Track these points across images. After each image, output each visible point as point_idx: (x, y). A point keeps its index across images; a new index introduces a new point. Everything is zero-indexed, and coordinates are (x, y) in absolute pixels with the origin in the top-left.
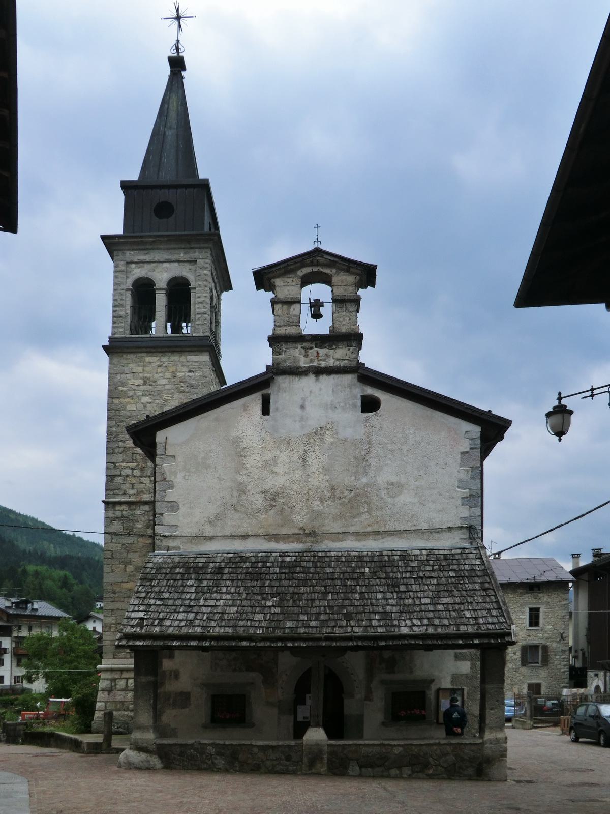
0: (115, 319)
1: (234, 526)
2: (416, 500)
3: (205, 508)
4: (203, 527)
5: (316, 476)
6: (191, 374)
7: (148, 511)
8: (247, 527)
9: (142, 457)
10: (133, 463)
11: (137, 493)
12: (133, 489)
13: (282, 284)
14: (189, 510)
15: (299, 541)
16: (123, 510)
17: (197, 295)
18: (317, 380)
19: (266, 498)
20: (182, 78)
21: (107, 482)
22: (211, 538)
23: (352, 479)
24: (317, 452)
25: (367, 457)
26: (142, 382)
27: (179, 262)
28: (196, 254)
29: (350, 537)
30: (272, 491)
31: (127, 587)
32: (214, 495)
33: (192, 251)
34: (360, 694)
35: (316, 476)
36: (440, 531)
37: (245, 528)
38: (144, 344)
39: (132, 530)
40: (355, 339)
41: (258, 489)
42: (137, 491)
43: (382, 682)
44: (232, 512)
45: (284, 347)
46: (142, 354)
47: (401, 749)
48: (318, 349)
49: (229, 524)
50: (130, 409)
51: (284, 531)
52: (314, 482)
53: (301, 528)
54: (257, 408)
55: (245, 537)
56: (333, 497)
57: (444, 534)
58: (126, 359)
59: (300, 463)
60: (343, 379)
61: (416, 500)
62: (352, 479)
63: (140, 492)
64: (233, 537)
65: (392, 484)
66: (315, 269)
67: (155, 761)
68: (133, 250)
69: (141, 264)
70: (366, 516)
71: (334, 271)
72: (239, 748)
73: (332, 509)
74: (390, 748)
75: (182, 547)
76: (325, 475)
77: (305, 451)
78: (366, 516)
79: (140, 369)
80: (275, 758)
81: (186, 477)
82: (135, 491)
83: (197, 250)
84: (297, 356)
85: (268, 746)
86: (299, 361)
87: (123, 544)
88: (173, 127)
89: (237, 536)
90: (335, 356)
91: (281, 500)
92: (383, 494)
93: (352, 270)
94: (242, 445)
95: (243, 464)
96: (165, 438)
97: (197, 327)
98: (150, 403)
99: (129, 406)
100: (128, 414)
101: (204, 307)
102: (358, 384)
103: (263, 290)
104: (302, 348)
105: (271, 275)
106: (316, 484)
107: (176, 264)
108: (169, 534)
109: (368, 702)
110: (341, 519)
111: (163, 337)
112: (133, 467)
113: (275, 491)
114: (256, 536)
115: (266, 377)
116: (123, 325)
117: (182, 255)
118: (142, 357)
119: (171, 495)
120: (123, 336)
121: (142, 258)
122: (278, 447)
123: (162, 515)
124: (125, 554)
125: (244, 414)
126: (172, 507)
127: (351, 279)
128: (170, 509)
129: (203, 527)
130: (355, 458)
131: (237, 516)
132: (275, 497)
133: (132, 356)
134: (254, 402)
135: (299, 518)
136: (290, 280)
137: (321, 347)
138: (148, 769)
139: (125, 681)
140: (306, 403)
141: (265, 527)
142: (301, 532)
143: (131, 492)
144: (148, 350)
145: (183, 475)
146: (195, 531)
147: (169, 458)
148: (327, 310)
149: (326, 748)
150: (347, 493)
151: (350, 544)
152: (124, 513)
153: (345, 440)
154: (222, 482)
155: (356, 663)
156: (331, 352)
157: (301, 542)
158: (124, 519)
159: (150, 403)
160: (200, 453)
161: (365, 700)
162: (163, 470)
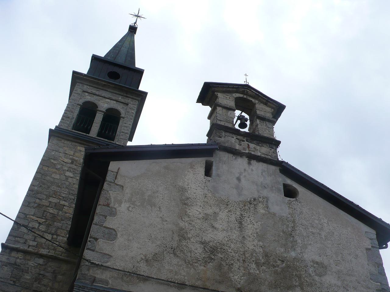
0: (64, 118)
1: (171, 271)
2: (339, 283)
3: (143, 244)
4: (138, 265)
5: (251, 239)
7: (41, 265)
8: (184, 276)
9: (51, 216)
10: (43, 219)
11: (36, 246)
12: (34, 241)
13: (223, 97)
14: (126, 242)
16: (18, 258)
17: (124, 122)
18: (249, 163)
19: (205, 249)
25: (293, 234)
27: (117, 101)
30: (211, 244)
32: (155, 233)
33: (127, 98)
35: (251, 239)
41: (198, 239)
42: (37, 244)
44: (171, 255)
46: (76, 144)
48: (250, 144)
49: (167, 267)
50: (55, 177)
52: (250, 245)
54: (202, 171)
58: (64, 143)
59: (237, 225)
60: (269, 167)
63: (39, 245)
65: (317, 263)
66: (245, 97)
69: (92, 95)
71: (257, 102)
75: (110, 282)
76: (259, 241)
77: (241, 215)
81: (130, 209)
83: (130, 99)
89: (174, 283)
92: (311, 270)
93: (269, 104)
96: (118, 168)
97: (120, 140)
98: (71, 178)
99: (54, 175)
100: (52, 180)
103: (201, 104)
104: (236, 138)
105: (216, 89)
106: (252, 247)
107: (115, 102)
108: (100, 263)
111: (95, 138)
112: (41, 222)
113: (214, 244)
116: (69, 123)
117: (120, 98)
118: (76, 146)
119: (111, 223)
120: (67, 129)
122: (218, 205)
123: (96, 239)
125: (190, 170)
128: (106, 236)
129: (138, 265)
131: (175, 261)
132: (214, 250)
134: (199, 163)
135: (236, 277)
141: (203, 280)
144: (82, 142)
145: (128, 206)
146: (129, 267)
147: (117, 187)
150: (279, 262)
152: (18, 260)
153: (274, 214)
154: (164, 223)
156: (258, 148)
158: (16, 267)
159: (71, 178)
160: (147, 190)
162: (109, 196)
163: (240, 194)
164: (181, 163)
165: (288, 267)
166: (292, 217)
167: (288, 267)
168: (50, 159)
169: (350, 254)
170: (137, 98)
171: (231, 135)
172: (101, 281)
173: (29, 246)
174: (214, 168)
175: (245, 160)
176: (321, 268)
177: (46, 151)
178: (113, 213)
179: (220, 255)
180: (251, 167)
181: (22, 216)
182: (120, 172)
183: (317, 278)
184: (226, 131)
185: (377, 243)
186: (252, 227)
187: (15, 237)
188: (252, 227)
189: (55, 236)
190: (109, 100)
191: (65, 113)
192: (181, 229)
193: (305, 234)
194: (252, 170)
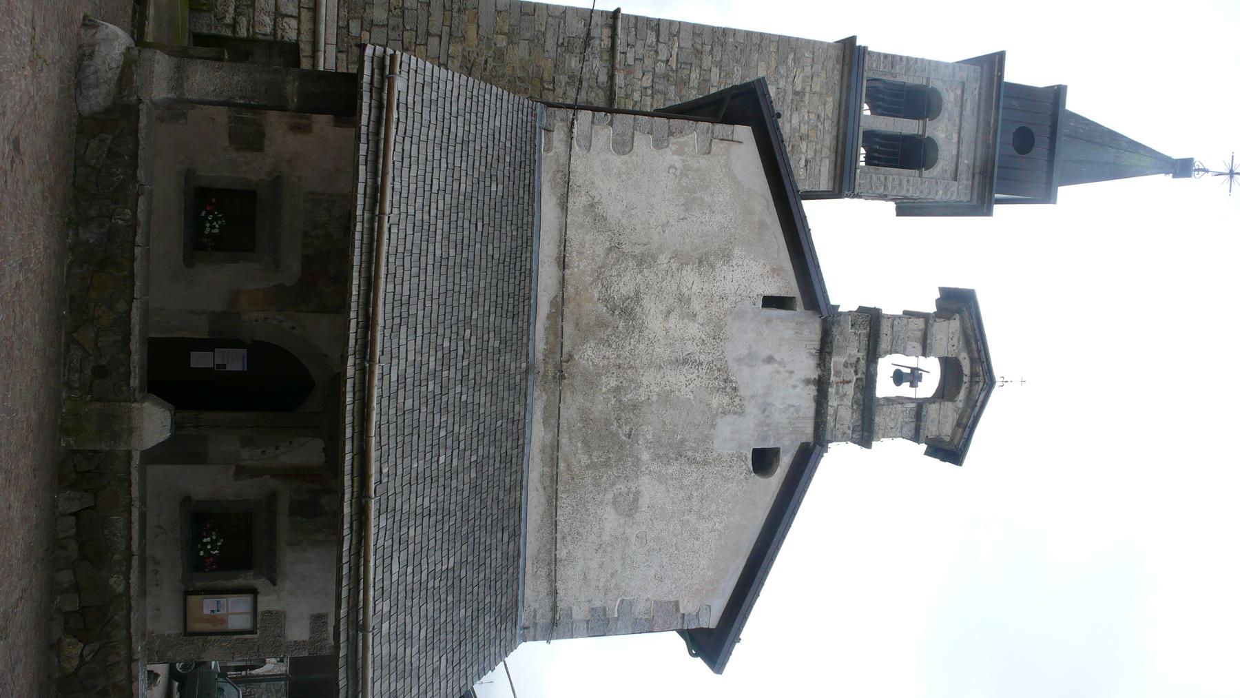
2: (606, 538)
6: (803, 163)
12: (635, 59)
15: (549, 352)
18: (808, 382)
20: (1167, 173)
21: (648, 20)
22: (564, 206)
23: (649, 437)
24: (697, 382)
25: (683, 460)
26: (798, 89)
27: (958, 156)
28: (965, 180)
29: (549, 436)
30: (638, 309)
31: (470, 32)
34: (249, 457)
36: (552, 578)
37: (580, 266)
38: (852, 97)
39: (567, 50)
40: (865, 436)
41: (643, 287)
43: (273, 497)
45: (863, 332)
46: (837, 93)
47: (120, 589)
49: (587, 238)
51: (568, 329)
52: (648, 377)
53: (571, 356)
54: (773, 290)
55: (562, 263)
56: (621, 407)
57: (546, 585)
58: (833, 69)
59: (681, 356)
61: (606, 538)
62: (649, 437)
63: (629, 70)
64: (564, 242)
65: (636, 500)
66: (966, 379)
67: (97, 99)
68: (980, 93)
70: (585, 460)
71: (961, 405)
72: (126, 273)
73: (601, 405)
74: (123, 568)
76: (659, 395)
78: (585, 460)
79: (817, 88)
80: (99, 345)
81: (672, 170)
82: (630, 61)
84: (850, 349)
85: (130, 334)
86: (839, 354)
87: (544, 34)
88: (1110, 155)
90: (842, 406)
91: (621, 324)
92: (621, 487)
93: (960, 430)
94: (719, 264)
95: (687, 264)
100: (753, 64)
101: (893, 188)
102: (797, 445)
107: (954, 152)
108: (575, 135)
109: (232, 472)
110: (582, 420)
114: (563, 282)
115: (822, 306)
119: (642, 143)
121: (969, 106)
122: (711, 320)
123: (611, 124)
124: (528, 35)
125: (768, 268)
126: (624, 144)
127: (947, 430)
130: (682, 441)
131: (600, 250)
132: (628, 314)
133: (837, 77)
134: (786, 285)
135: (590, 352)
136: (955, 341)
137: (856, 387)
138: (78, 85)
139: (295, 13)
140: (776, 365)
142: (565, 357)
143: (630, 56)
144: (844, 103)
145: (677, 165)
146: (577, 179)
148: (905, 390)
149: (123, 447)
151: (538, 434)
152: (597, 42)
153: (713, 426)
155: (308, 452)
156: (848, 402)
157: (545, 355)
160: (712, 195)
161: (238, 466)
163: (739, 360)
164: (778, 252)
165: (621, 445)
166: (714, 460)
167: (621, 445)
168: (794, 50)
169: (661, 566)
170: (975, 197)
171: (864, 347)
172: (549, 141)
173: (625, 53)
174: (783, 312)
175: (814, 374)
176: (629, 506)
177: (809, 41)
178: (659, 144)
179: (621, 324)
180: (801, 385)
181: (675, 29)
182: (734, 145)
183: (609, 496)
184: (869, 336)
185: (693, 627)
186: (682, 382)
187: (636, 27)
188: (682, 382)
189: (649, 92)
190: (955, 139)
191: (901, 58)
192: (655, 258)
193: (685, 482)
194: (794, 387)
